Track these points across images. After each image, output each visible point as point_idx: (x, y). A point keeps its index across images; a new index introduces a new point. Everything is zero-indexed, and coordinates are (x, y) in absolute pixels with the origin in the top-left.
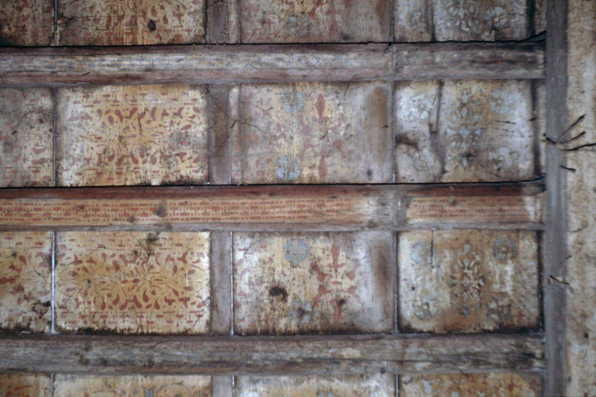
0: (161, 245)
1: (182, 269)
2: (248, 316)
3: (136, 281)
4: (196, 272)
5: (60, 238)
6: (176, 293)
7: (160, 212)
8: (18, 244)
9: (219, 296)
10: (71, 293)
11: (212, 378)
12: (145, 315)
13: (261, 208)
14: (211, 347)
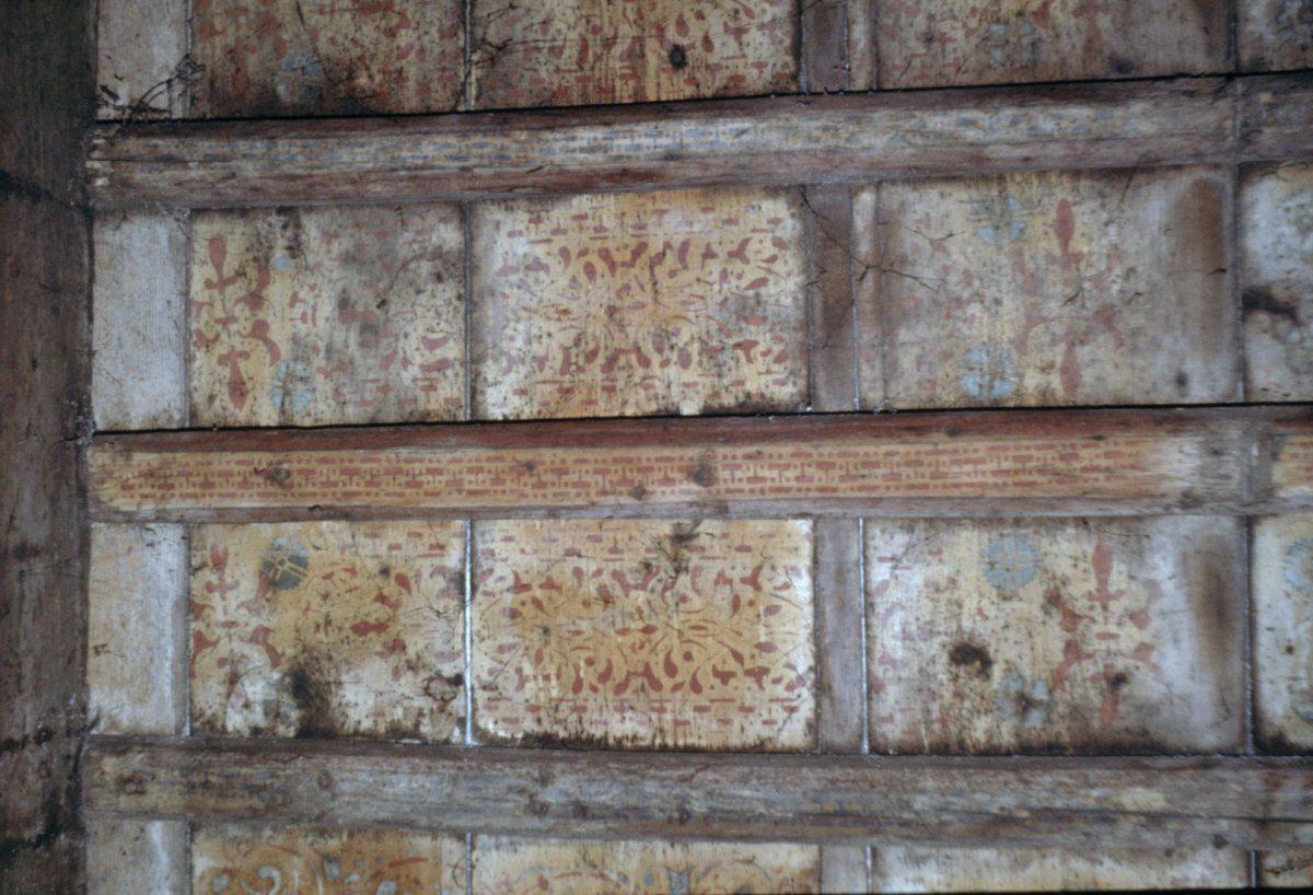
0: (703, 549)
1: (751, 603)
2: (901, 710)
3: (648, 630)
5: (483, 534)
6: (738, 657)
8: (391, 548)
9: (834, 665)
10: (506, 657)
11: (821, 852)
12: (669, 706)
13: (930, 465)
14: (818, 779)
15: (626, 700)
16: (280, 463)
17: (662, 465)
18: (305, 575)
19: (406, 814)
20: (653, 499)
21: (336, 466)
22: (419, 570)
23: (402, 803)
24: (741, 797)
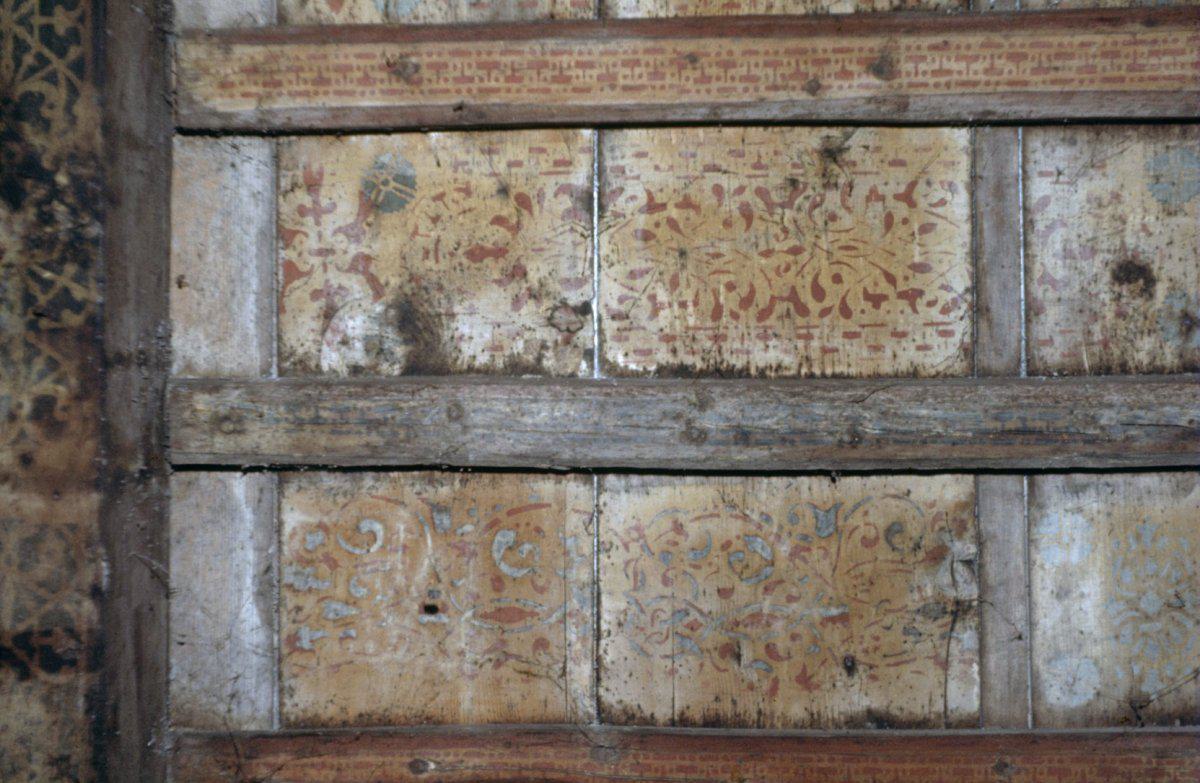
0: (854, 164)
1: (905, 221)
2: (1062, 332)
3: (796, 251)
4: (938, 228)
5: (612, 149)
6: (891, 279)
7: (882, 67)
8: (510, 165)
9: (992, 285)
10: (639, 283)
11: (976, 484)
12: (816, 332)
13: (1127, 56)
14: (1000, 396)
15: (771, 327)
16: (408, 55)
17: (840, 56)
18: (412, 196)
19: (548, 445)
20: (828, 94)
21: (473, 59)
22: (541, 189)
23: (543, 433)
24: (918, 417)
